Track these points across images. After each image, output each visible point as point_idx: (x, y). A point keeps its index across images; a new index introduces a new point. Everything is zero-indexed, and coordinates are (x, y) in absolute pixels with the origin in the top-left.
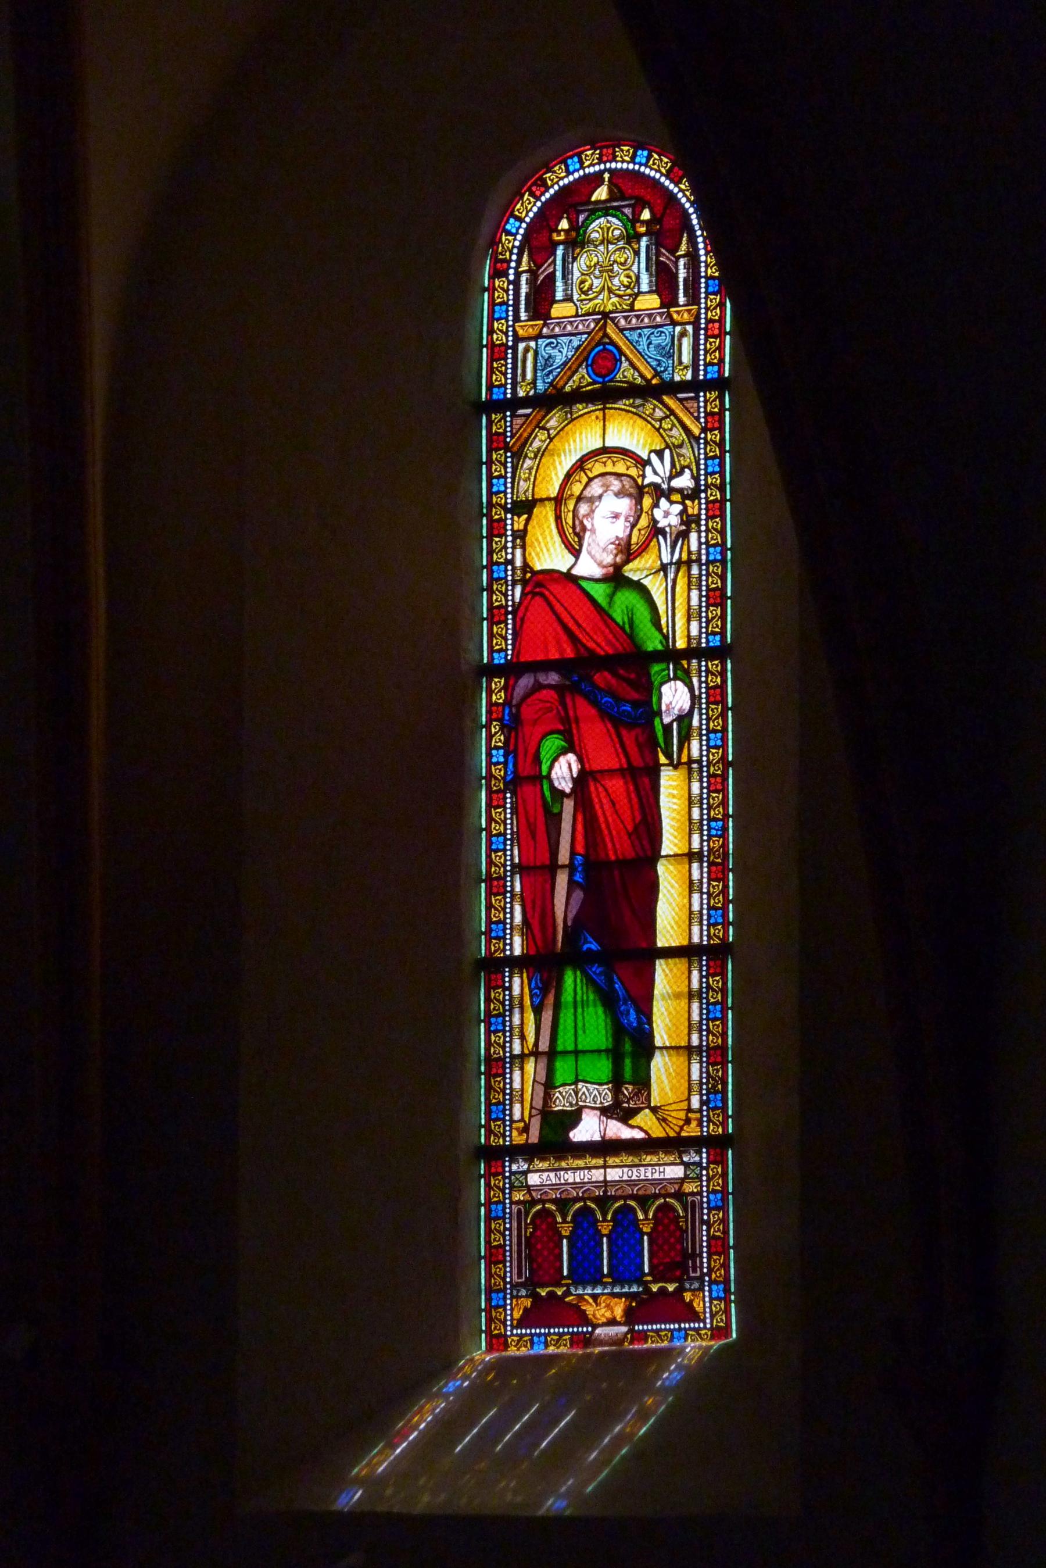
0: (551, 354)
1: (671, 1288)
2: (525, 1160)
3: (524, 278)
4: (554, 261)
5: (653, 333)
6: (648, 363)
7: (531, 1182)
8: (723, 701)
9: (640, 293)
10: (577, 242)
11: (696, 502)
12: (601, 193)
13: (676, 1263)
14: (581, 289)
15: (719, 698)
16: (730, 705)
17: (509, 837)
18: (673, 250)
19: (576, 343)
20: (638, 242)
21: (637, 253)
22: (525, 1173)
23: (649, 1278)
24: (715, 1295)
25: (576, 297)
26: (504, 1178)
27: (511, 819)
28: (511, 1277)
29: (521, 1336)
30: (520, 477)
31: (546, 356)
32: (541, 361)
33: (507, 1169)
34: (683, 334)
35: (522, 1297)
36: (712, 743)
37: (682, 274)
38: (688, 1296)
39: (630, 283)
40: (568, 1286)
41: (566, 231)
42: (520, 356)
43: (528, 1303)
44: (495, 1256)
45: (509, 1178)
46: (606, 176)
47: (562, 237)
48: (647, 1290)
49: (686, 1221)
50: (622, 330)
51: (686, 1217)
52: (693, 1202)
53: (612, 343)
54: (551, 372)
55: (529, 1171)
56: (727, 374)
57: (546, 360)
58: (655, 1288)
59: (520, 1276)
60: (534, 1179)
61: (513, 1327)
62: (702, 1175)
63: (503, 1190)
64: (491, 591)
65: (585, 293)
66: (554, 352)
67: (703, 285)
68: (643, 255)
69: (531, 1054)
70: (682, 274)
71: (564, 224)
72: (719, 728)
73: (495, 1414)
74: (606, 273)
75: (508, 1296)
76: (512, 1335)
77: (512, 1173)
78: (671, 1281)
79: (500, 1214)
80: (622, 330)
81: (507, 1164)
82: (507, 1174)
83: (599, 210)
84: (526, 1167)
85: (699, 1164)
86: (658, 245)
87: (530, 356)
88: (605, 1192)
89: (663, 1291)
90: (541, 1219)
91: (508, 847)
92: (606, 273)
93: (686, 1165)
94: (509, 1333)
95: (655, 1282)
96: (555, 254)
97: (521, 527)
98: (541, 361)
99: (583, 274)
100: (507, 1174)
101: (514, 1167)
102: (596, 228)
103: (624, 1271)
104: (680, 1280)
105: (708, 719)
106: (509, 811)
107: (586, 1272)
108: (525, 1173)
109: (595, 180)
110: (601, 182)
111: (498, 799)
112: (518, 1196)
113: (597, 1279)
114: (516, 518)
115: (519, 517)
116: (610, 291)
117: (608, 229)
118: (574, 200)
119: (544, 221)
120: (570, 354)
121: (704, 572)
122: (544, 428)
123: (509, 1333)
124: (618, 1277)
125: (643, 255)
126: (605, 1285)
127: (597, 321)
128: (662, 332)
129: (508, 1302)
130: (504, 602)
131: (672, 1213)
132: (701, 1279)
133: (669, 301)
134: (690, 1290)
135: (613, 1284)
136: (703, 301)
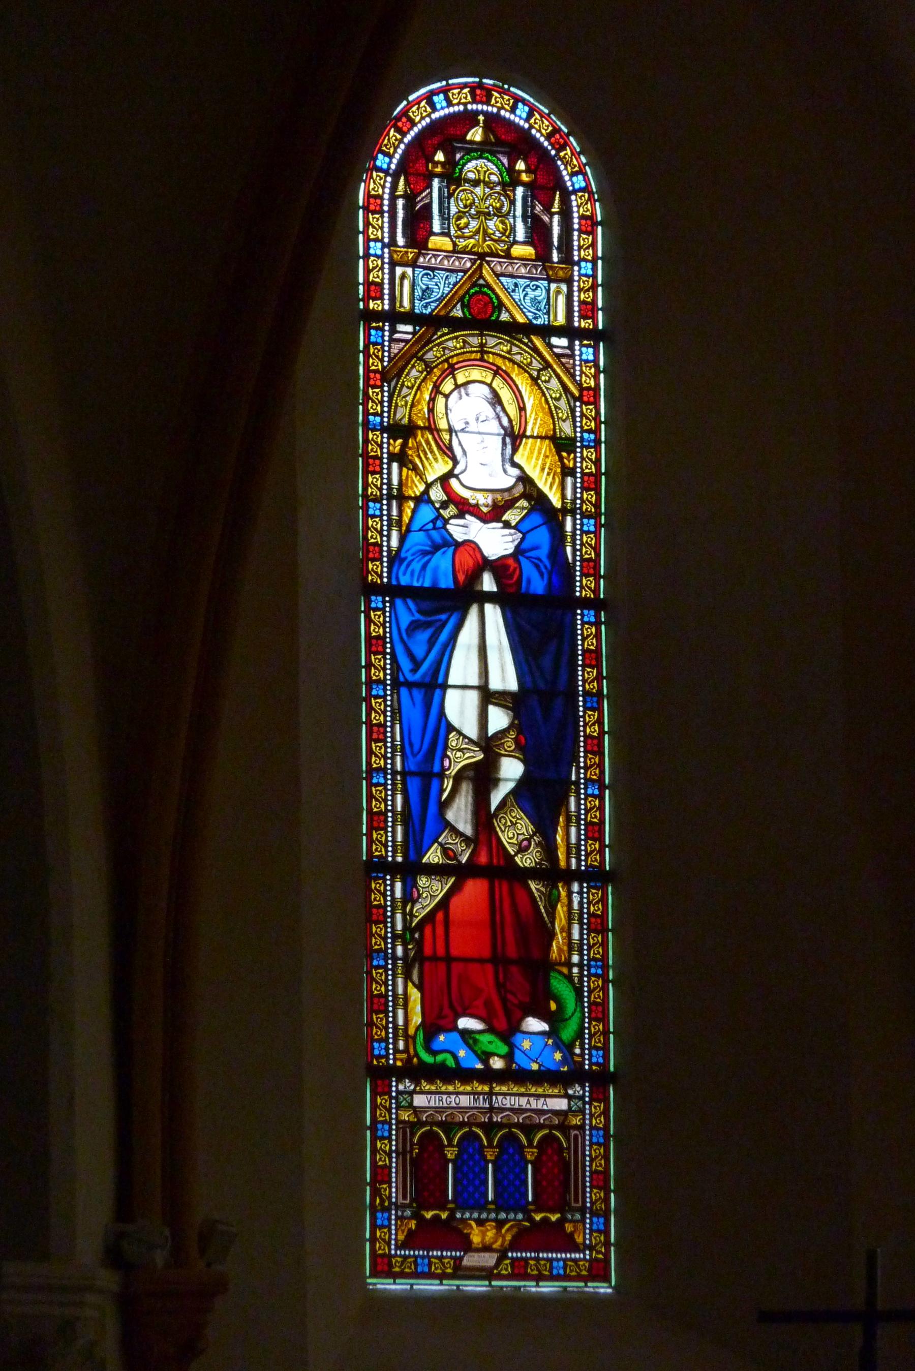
0: (426, 286)
1: (554, 1218)
2: (411, 1081)
3: (400, 203)
4: (430, 193)
5: (528, 286)
6: (524, 313)
7: (416, 1104)
8: (601, 839)
9: (515, 242)
10: (453, 179)
11: (572, 456)
12: (476, 135)
13: (559, 1184)
14: (458, 226)
15: (600, 1015)
16: (607, 843)
17: (389, 787)
18: (548, 208)
19: (452, 280)
20: (514, 191)
21: (513, 202)
22: (411, 1094)
23: (531, 1207)
24: (595, 1140)
25: (453, 232)
26: (391, 1098)
27: (391, 695)
28: (396, 1198)
29: (405, 1257)
30: (396, 404)
31: (424, 287)
32: (418, 293)
33: (394, 1089)
34: (558, 292)
35: (406, 1218)
36: (595, 1227)
37: (556, 230)
38: (569, 1228)
39: (506, 230)
40: (451, 1210)
41: (443, 164)
42: (397, 281)
43: (413, 1224)
44: (381, 1175)
45: (396, 1098)
46: (481, 118)
47: (439, 169)
48: (531, 1220)
49: (569, 1153)
50: (498, 276)
51: (569, 1148)
52: (576, 1137)
53: (488, 286)
54: (429, 303)
55: (414, 1092)
56: (600, 327)
57: (424, 291)
58: (538, 1217)
59: (405, 1197)
60: (419, 1101)
61: (397, 1248)
62: (585, 1109)
63: (385, 939)
64: (367, 356)
65: (460, 229)
66: (431, 284)
67: (580, 673)
68: (519, 204)
69: (414, 959)
70: (556, 230)
71: (440, 157)
72: (601, 1126)
73: (359, 345)
74: (481, 207)
75: (393, 1217)
76: (396, 1255)
77: (399, 1092)
78: (553, 1211)
79: (386, 1134)
80: (498, 276)
81: (394, 1084)
82: (394, 1094)
83: (475, 150)
84: (412, 1087)
85: (582, 1098)
86: (534, 197)
87: (407, 284)
88: (490, 1118)
89: (545, 1220)
90: (425, 1149)
91: (385, 512)
92: (481, 207)
93: (570, 1098)
94: (393, 1252)
95: (537, 1211)
96: (430, 186)
97: (397, 449)
98: (418, 293)
99: (460, 211)
100: (394, 1094)
101: (401, 1087)
102: (472, 167)
103: (510, 1198)
104: (562, 1212)
105: (589, 903)
106: (385, 564)
107: (469, 1197)
108: (411, 1094)
109: (469, 119)
110: (477, 123)
111: (378, 733)
112: (405, 1116)
113: (482, 1205)
114: (391, 441)
115: (395, 441)
116: (486, 234)
117: (485, 172)
118: (447, 133)
119: (419, 150)
120: (447, 290)
121: (585, 900)
122: (421, 359)
123: (393, 1252)
124: (501, 1204)
125: (519, 204)
126: (489, 1211)
127: (473, 262)
128: (537, 287)
129: (393, 1222)
130: (379, 453)
131: (555, 1147)
132: (583, 1210)
133: (543, 256)
134: (571, 1221)
135: (497, 1211)
136: (582, 760)
